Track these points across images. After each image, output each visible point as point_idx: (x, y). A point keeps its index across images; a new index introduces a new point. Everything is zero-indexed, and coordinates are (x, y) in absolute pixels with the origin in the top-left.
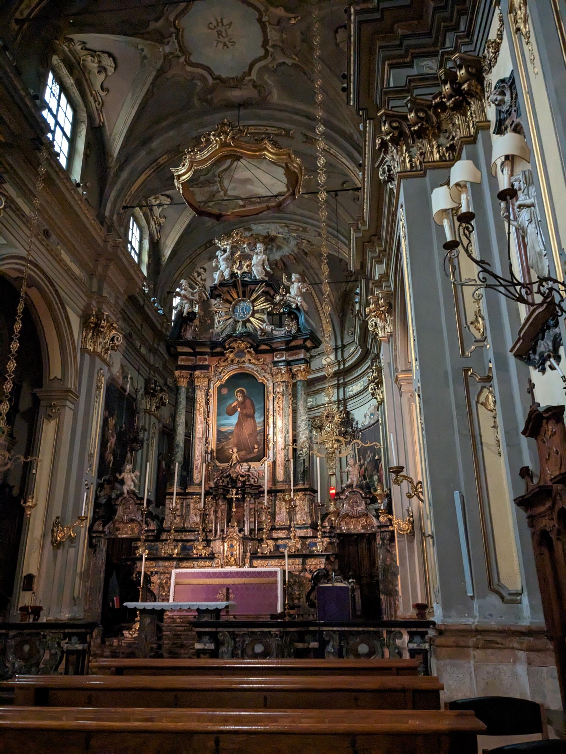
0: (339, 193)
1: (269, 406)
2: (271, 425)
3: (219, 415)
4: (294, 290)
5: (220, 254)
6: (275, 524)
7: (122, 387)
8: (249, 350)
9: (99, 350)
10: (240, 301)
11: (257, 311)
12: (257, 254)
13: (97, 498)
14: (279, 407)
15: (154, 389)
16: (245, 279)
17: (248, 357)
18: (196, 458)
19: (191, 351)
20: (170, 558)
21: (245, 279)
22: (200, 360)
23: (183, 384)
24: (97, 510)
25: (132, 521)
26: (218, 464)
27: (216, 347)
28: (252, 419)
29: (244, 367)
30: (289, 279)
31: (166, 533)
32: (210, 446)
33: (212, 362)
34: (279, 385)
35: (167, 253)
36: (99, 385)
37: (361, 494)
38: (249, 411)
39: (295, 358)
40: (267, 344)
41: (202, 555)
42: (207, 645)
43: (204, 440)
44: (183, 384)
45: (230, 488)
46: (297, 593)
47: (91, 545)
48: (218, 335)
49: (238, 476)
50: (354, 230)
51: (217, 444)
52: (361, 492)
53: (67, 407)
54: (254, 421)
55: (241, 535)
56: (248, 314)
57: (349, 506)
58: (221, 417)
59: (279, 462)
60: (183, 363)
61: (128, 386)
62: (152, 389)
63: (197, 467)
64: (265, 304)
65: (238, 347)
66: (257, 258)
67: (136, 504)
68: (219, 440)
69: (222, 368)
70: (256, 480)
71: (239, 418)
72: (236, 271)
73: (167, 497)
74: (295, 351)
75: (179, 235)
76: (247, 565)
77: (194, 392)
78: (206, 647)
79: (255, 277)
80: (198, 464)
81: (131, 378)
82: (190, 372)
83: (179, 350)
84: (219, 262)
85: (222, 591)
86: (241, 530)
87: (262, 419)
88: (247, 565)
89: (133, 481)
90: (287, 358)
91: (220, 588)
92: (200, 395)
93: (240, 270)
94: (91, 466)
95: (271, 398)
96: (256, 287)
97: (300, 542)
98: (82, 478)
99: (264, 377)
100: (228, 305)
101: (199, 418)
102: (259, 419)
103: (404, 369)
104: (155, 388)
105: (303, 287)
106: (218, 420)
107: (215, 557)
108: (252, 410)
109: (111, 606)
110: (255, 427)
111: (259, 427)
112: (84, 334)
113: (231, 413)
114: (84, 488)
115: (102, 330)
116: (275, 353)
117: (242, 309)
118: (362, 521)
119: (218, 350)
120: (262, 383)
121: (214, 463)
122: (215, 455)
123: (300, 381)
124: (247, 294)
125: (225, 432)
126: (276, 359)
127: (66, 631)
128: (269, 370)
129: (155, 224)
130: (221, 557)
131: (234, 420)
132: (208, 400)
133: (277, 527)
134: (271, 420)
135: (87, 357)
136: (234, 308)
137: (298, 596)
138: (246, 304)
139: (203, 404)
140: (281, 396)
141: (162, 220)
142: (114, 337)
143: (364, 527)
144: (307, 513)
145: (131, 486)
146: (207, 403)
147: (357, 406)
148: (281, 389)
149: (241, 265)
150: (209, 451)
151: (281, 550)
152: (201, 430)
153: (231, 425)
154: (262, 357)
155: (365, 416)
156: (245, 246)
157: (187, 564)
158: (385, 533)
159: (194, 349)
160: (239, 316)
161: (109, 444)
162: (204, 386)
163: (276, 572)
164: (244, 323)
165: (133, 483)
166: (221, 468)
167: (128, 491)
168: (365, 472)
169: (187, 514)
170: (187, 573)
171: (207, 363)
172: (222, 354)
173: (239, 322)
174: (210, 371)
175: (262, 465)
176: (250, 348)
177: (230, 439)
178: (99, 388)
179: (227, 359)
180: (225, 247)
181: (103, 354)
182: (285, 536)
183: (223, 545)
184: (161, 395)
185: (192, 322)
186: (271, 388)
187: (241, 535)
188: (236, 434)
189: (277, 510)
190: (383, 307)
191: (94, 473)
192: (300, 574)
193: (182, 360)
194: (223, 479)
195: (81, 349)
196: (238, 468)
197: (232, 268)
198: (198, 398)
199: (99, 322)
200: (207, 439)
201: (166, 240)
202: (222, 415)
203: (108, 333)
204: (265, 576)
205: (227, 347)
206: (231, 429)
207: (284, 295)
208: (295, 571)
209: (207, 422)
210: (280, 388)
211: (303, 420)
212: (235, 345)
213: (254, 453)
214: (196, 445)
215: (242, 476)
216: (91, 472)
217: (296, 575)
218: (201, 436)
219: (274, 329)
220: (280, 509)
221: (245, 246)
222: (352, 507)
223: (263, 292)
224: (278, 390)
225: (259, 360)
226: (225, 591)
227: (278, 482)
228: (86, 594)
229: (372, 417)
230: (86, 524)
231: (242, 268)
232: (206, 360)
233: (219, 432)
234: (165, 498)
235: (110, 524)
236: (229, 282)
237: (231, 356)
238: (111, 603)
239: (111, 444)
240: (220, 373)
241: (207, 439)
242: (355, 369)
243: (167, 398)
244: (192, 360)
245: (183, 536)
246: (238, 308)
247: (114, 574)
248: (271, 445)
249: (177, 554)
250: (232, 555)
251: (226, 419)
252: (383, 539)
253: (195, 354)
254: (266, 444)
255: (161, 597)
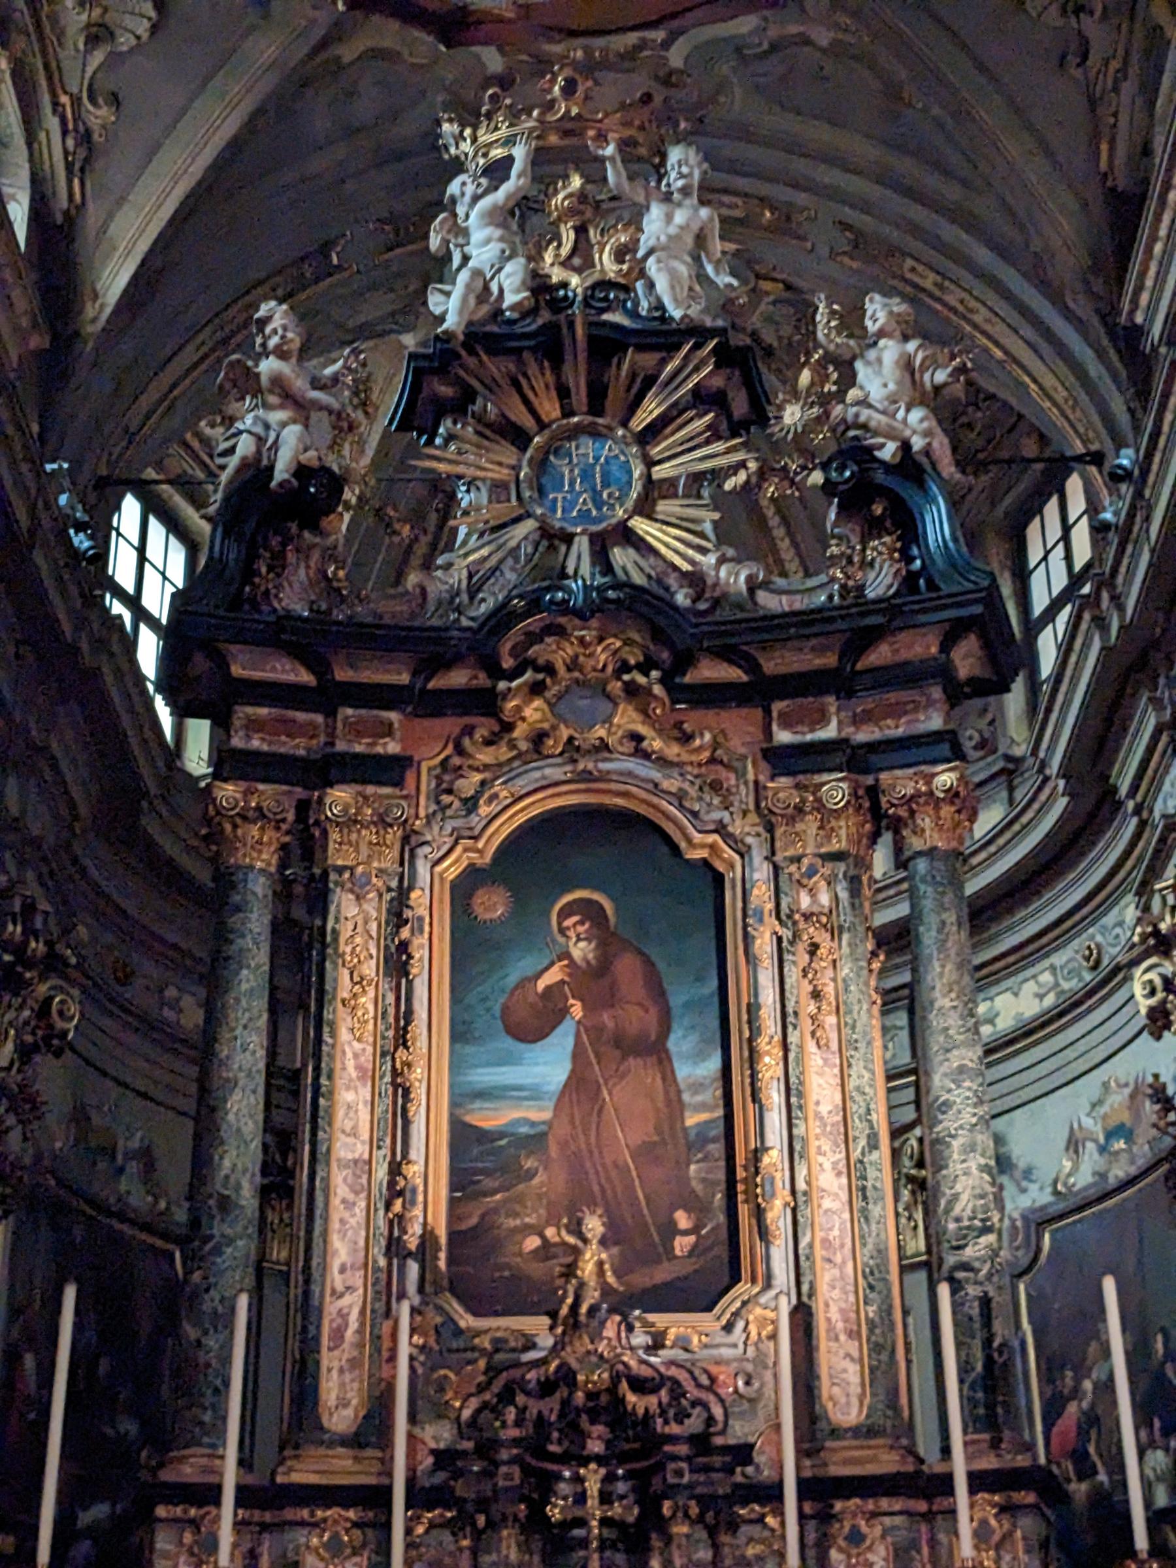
2: (774, 1097)
3: (460, 1034)
5: (470, 189)
8: (641, 680)
10: (575, 432)
11: (668, 488)
12: (667, 198)
14: (816, 995)
16: (606, 317)
17: (627, 718)
18: (337, 1280)
19: (305, 677)
21: (606, 317)
22: (357, 730)
26: (466, 1320)
27: (447, 664)
29: (604, 777)
32: (418, 1212)
34: (812, 872)
39: (896, 729)
40: (727, 654)
43: (381, 1173)
48: (450, 601)
49: (615, 1379)
51: (453, 1203)
54: (668, 1076)
56: (621, 500)
58: (469, 1049)
59: (834, 1315)
63: (338, 1335)
64: (719, 447)
65: (573, 665)
66: (669, 218)
69: (477, 777)
71: (578, 1055)
72: (557, 275)
73: (161, 1511)
74: (893, 697)
77: (319, 900)
80: (343, 1315)
82: (299, 792)
83: (236, 670)
84: (465, 232)
87: (714, 1064)
90: (849, 731)
93: (579, 271)
95: (764, 945)
96: (663, 362)
99: (720, 829)
100: (509, 454)
104: (26, 943)
106: (456, 1066)
108: (654, 1012)
110: (675, 1106)
111: (702, 1107)
119: (458, 678)
121: (440, 1309)
122: (442, 1264)
123: (931, 853)
124: (615, 397)
125: (501, 1135)
126: (783, 737)
128: (745, 796)
129: (65, 133)
132: (404, 946)
134: (770, 1065)
136: (541, 465)
138: (607, 448)
139: (369, 969)
140: (823, 938)
141: (98, 116)
147: (1025, 1095)
148: (825, 899)
149: (582, 246)
150: (412, 1243)
152: (364, 1115)
155: (1074, 1145)
156: (610, 150)
159: (319, 666)
162: (381, 872)
166: (485, 1343)
171: (392, 747)
175: (728, 1328)
176: (644, 667)
177: (531, 1175)
179: (508, 727)
184: (43, 989)
185: (316, 528)
186: (762, 894)
188: (563, 1145)
193: (254, 725)
194: (520, 1399)
197: (535, 257)
198: (346, 931)
200: (395, 1170)
201: (110, 216)
205: (507, 663)
206: (534, 1116)
207: (825, 401)
209: (395, 1073)
210: (812, 892)
211: (962, 1069)
212: (556, 652)
213: (671, 1257)
214: (335, 1202)
215: (640, 1385)
218: (361, 1150)
219: (766, 585)
221: (610, 150)
223: (696, 391)
224: (805, 901)
225: (686, 739)
227: (835, 1432)
231: (589, 264)
232: (387, 730)
234: (151, 1521)
236: (518, 329)
237: (534, 712)
240: (471, 804)
241: (395, 1170)
242: (1010, 911)
243: (73, 1009)
244: (310, 731)
248: (777, 1214)
251: (507, 1060)
254: (744, 1210)
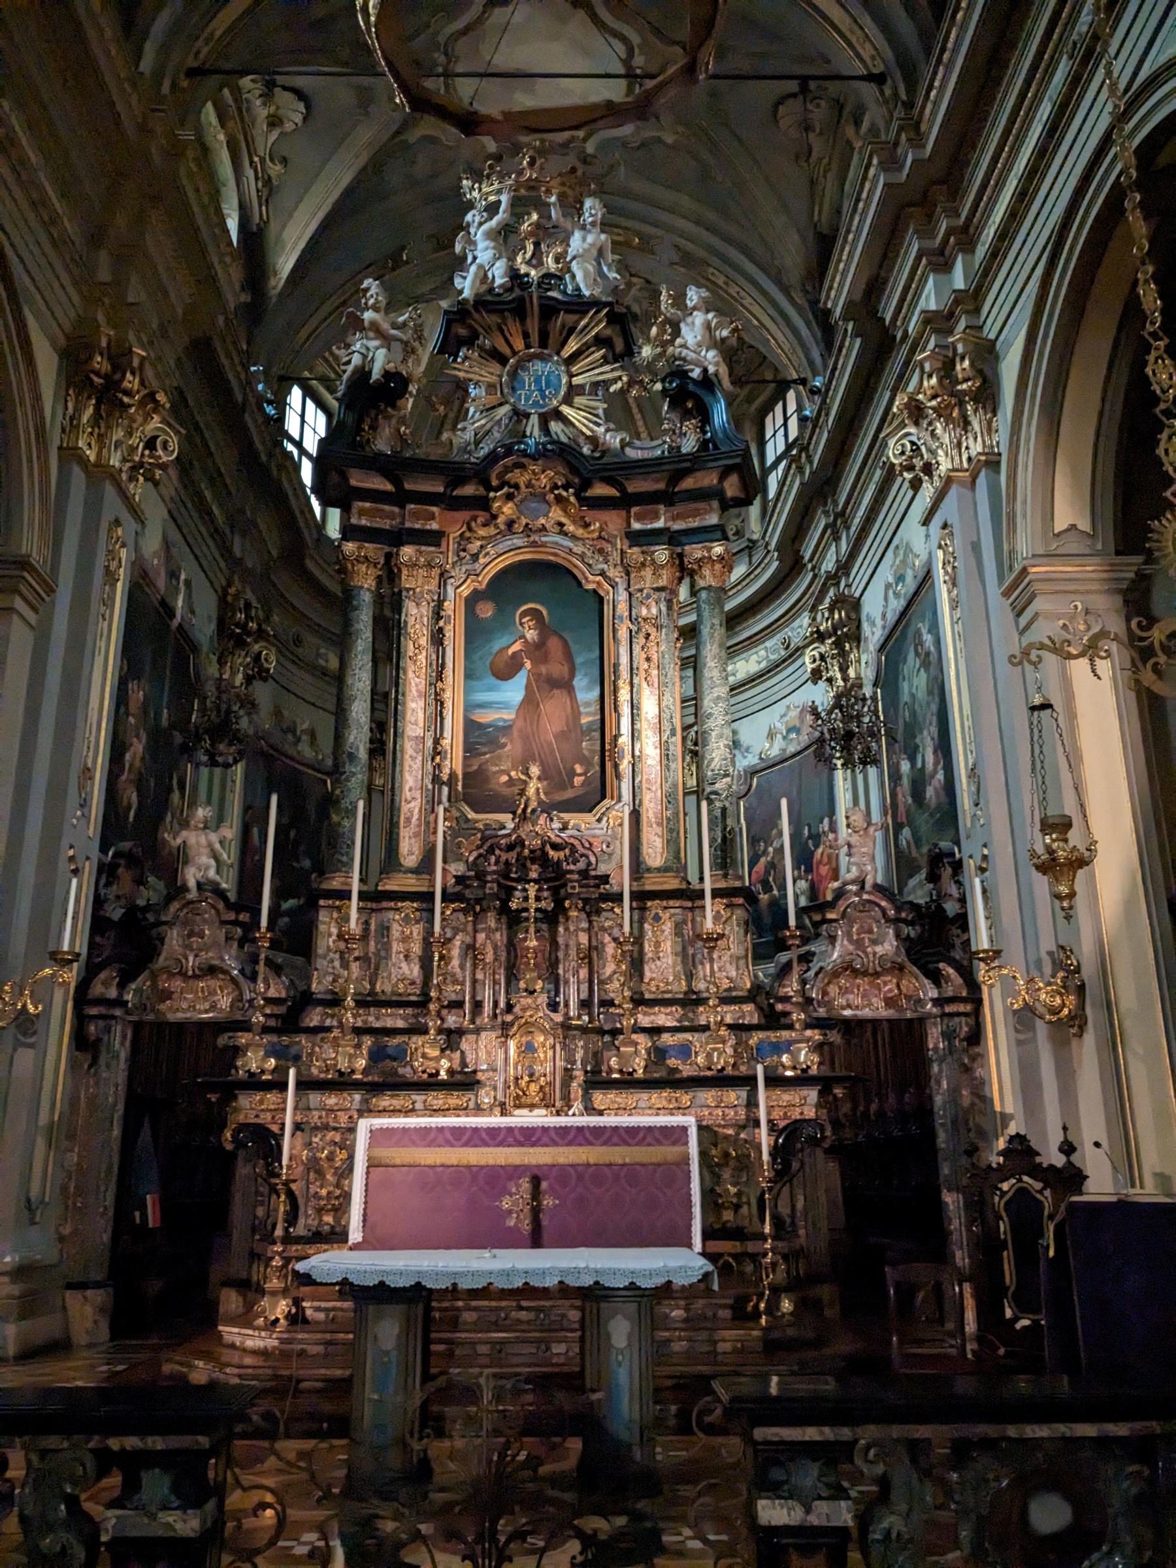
0: (812, 85)
1: (618, 656)
2: (625, 710)
3: (469, 676)
4: (692, 333)
5: (477, 219)
6: (644, 987)
7: (163, 603)
9: (115, 461)
10: (531, 358)
12: (583, 228)
13: (98, 902)
14: (648, 659)
15: (244, 626)
17: (556, 514)
19: (389, 487)
20: (341, 1083)
22: (416, 516)
23: (366, 580)
24: (98, 939)
25: (211, 971)
26: (471, 815)
28: (565, 693)
29: (544, 545)
30: (679, 299)
31: (319, 1009)
32: (448, 762)
33: (452, 524)
34: (648, 597)
35: (285, 264)
36: (112, 568)
37: (884, 911)
38: (557, 669)
39: (694, 523)
41: (438, 1073)
42: (822, 1507)
43: (429, 743)
44: (366, 580)
45: (513, 880)
46: (733, 1190)
47: (82, 1042)
48: (464, 449)
49: (544, 844)
50: (880, 163)
52: (883, 904)
53: (15, 618)
55: (558, 1018)
56: (556, 395)
57: (850, 941)
58: (474, 683)
59: (651, 814)
60: (364, 522)
61: (180, 603)
62: (237, 625)
64: (607, 368)
65: (529, 485)
66: (584, 239)
67: (224, 923)
68: (470, 749)
69: (479, 543)
70: (593, 860)
71: (528, 687)
72: (523, 269)
73: (322, 902)
75: (321, 215)
76: (577, 1106)
77: (397, 607)
78: (814, 1520)
79: (578, 289)
80: (411, 812)
81: (188, 583)
82: (387, 549)
83: (353, 482)
84: (474, 243)
85: (518, 1186)
86: (553, 1006)
87: (596, 693)
88: (577, 1106)
89: (216, 857)
90: (669, 524)
91: (510, 1178)
92: (416, 616)
93: (535, 267)
94: (84, 804)
95: (623, 634)
97: (732, 1042)
98: (60, 839)
99: (602, 573)
100: (496, 368)
101: (415, 680)
102: (586, 694)
103: (1041, 552)
105: (720, 325)
106: (467, 692)
107: (478, 1082)
109: (138, 1221)
110: (576, 714)
111: (588, 714)
112: (70, 405)
113: (505, 671)
114: (64, 867)
115: (126, 400)
116: (634, 510)
117: (538, 381)
118: (885, 984)
119: (469, 490)
120: (595, 591)
121: (459, 810)
122: (460, 788)
124: (553, 339)
127: (114, 1444)
128: (616, 557)
129: (257, 179)
130: (500, 1080)
131: (514, 691)
132: (441, 630)
133: (647, 996)
134: (624, 695)
135: (78, 475)
136: (513, 375)
137: (735, 1200)
138: (548, 367)
139: (423, 641)
140: (653, 631)
141: (275, 169)
142: (155, 438)
143: (890, 1002)
144: (738, 958)
145: (207, 868)
146: (438, 639)
148: (654, 611)
150: (445, 778)
151: (672, 1062)
152: (421, 715)
153: (504, 705)
154: (601, 520)
155: (771, 735)
156: (553, 199)
157: (395, 1102)
158: (957, 1020)
159: (397, 482)
160: (527, 400)
161: (128, 757)
163: (684, 1129)
164: (544, 420)
165: (212, 862)
167: (199, 885)
168: (767, 872)
169: (383, 953)
170: (405, 1130)
171: (434, 526)
172: (483, 504)
173: (527, 416)
174: (443, 548)
175: (599, 820)
176: (566, 487)
177: (504, 745)
178: (110, 577)
179: (495, 517)
180: (492, 198)
181: (124, 476)
182: (675, 1024)
183: (504, 1045)
184: (256, 647)
185: (394, 407)
187: (558, 1018)
188: (520, 731)
189: (648, 948)
190: (966, 380)
191: (93, 829)
192: (738, 1134)
193: (362, 513)
194: (497, 852)
195: (60, 448)
196: (541, 821)
197: (512, 259)
198: (411, 621)
199: (117, 376)
200: (437, 742)
201: (284, 227)
202: (479, 679)
203: (140, 419)
204: (615, 1139)
205: (495, 483)
206: (506, 717)
207: (665, 344)
208: (724, 1127)
209: (436, 694)
210: (648, 607)
211: (719, 698)
214: (407, 757)
215: (555, 847)
216: (83, 821)
217: (727, 1137)
218: (419, 732)
219: (629, 444)
220: (657, 944)
221: (553, 199)
222: (859, 944)
223: (596, 336)
224: (644, 612)
225: (586, 525)
226: (525, 1185)
227: (649, 870)
228: (64, 1189)
229: (794, 736)
230: (71, 976)
231: (541, 264)
233: (471, 727)
235: (142, 982)
237: (508, 509)
238: (137, 1214)
239: (134, 757)
241: (437, 742)
243: (273, 658)
244: (392, 516)
245: (371, 1019)
246: (526, 377)
247: (146, 1124)
248: (625, 766)
249: (365, 1072)
250: (531, 1075)
251: (491, 689)
252: (948, 1035)
253: (401, 498)
254: (608, 765)
255: (313, 1202)
